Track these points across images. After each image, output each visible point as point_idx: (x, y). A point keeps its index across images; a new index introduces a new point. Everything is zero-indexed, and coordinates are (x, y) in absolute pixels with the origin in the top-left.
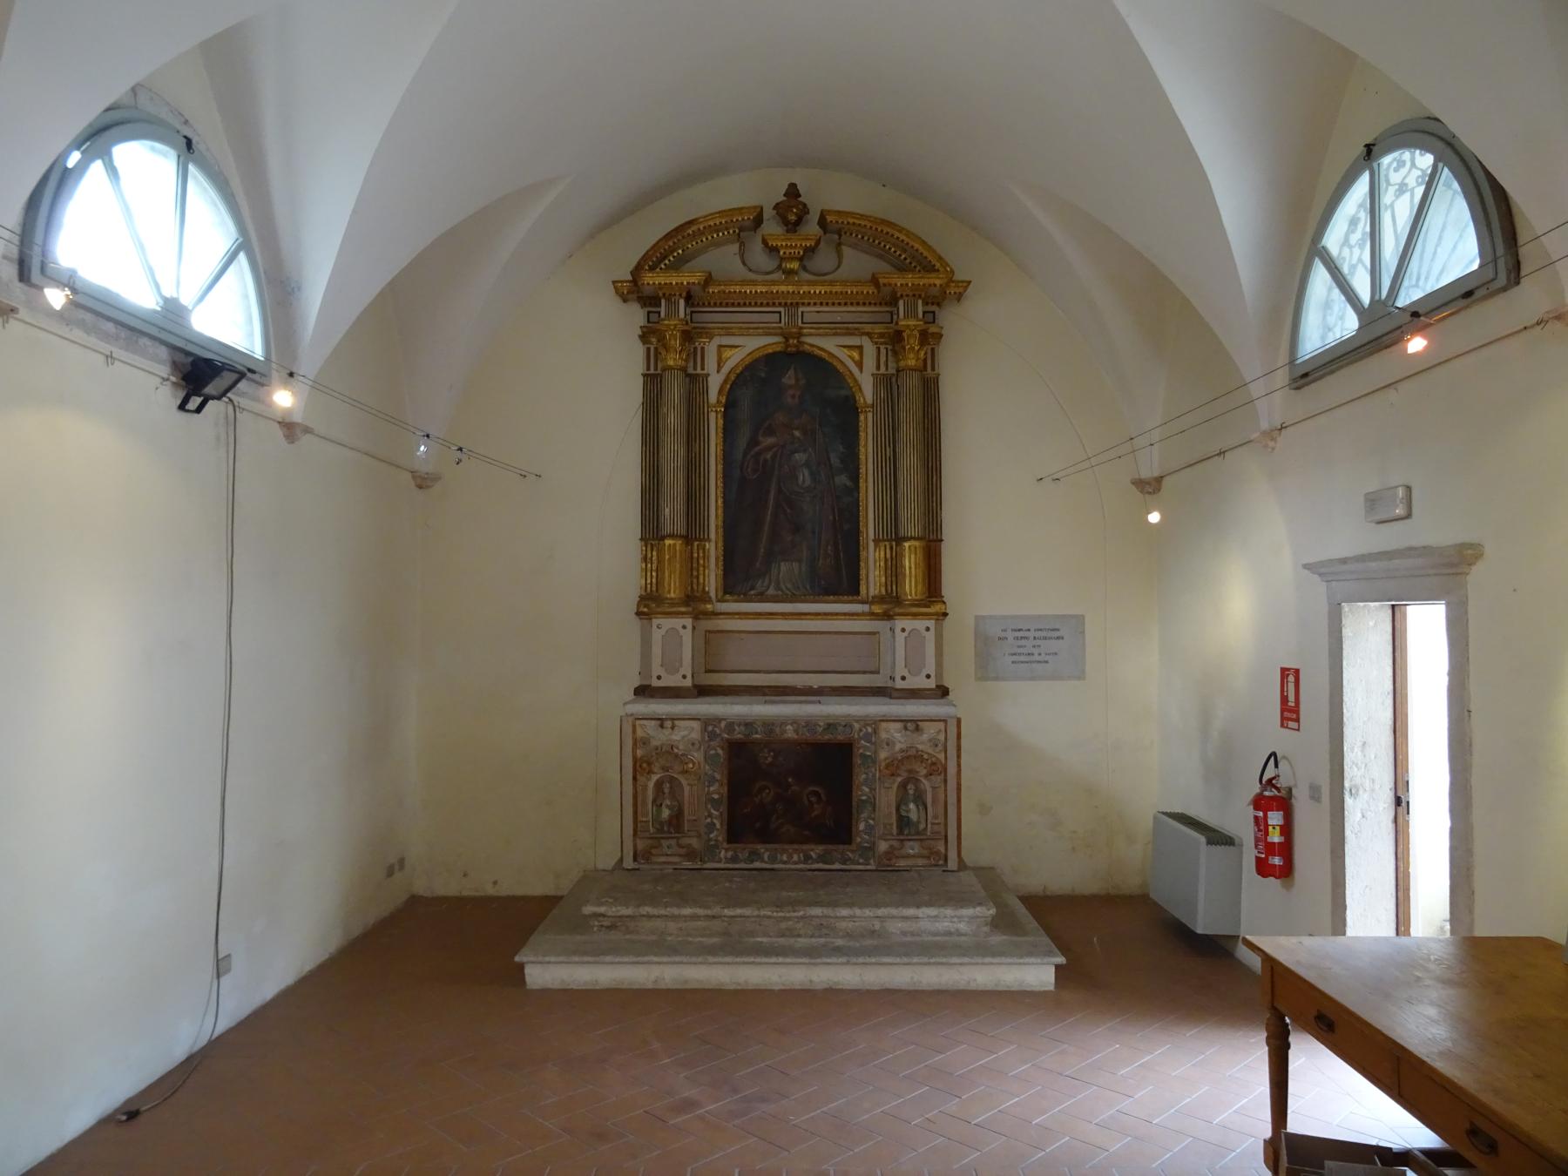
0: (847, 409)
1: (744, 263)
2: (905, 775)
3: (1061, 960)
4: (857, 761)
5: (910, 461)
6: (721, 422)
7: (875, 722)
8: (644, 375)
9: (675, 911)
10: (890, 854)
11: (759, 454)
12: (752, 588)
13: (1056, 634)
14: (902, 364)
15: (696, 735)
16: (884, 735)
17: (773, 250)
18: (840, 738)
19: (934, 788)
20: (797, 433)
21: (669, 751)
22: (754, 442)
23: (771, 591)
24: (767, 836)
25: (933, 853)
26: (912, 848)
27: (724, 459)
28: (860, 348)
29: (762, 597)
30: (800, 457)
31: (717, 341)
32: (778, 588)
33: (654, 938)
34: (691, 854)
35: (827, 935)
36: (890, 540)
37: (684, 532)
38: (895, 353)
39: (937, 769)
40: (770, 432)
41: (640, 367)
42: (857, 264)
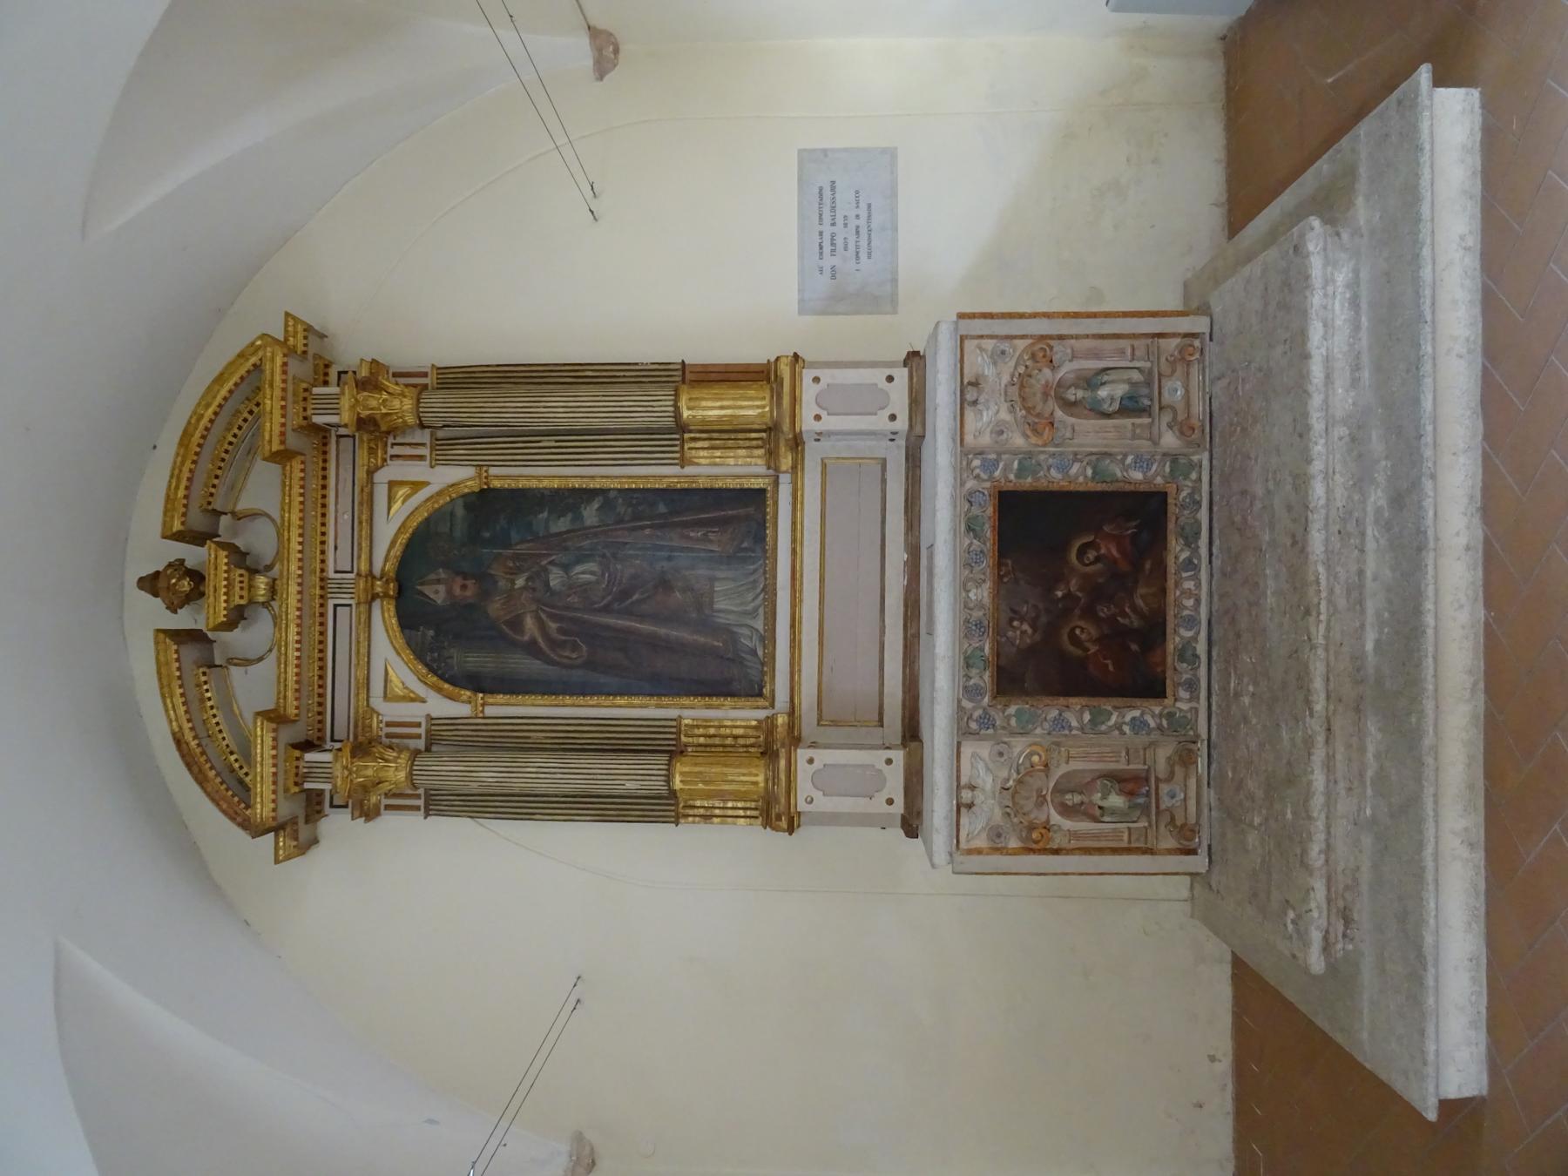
0: (489, 509)
1: (261, 659)
2: (1052, 404)
3: (1424, 73)
4: (1028, 483)
5: (558, 409)
6: (500, 698)
7: (965, 454)
8: (427, 815)
9: (1318, 801)
10: (1183, 428)
11: (554, 644)
12: (754, 653)
13: (827, 193)
14: (411, 419)
15: (985, 750)
16: (986, 440)
17: (237, 617)
18: (990, 511)
19: (1073, 357)
20: (520, 582)
21: (1012, 793)
22: (532, 649)
23: (759, 624)
24: (1154, 630)
25: (1182, 359)
26: (1174, 391)
27: (555, 693)
28: (392, 485)
29: (769, 638)
30: (556, 579)
31: (377, 702)
32: (753, 614)
33: (1367, 841)
34: (1185, 758)
35: (1359, 523)
36: (683, 441)
37: (664, 758)
38: (392, 431)
39: (1042, 350)
40: (516, 624)
41: (414, 820)
42: (262, 488)
